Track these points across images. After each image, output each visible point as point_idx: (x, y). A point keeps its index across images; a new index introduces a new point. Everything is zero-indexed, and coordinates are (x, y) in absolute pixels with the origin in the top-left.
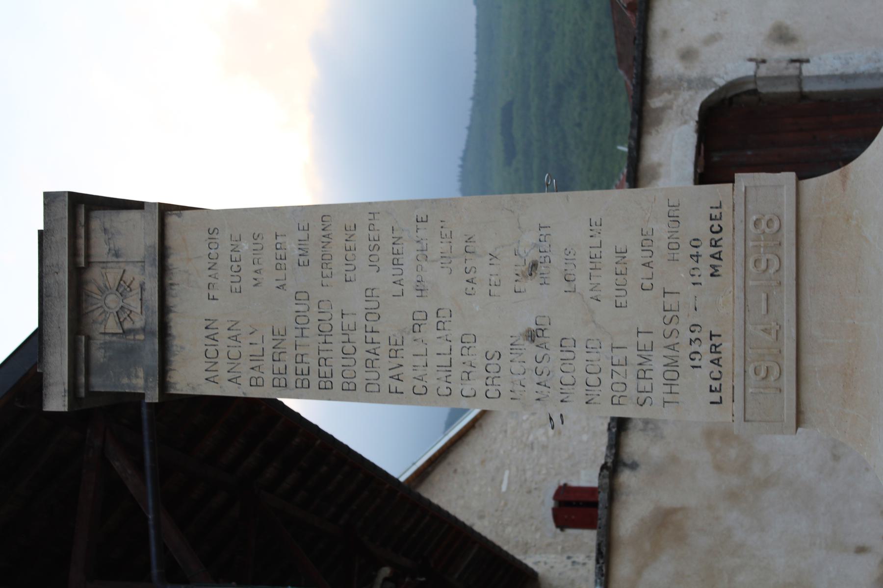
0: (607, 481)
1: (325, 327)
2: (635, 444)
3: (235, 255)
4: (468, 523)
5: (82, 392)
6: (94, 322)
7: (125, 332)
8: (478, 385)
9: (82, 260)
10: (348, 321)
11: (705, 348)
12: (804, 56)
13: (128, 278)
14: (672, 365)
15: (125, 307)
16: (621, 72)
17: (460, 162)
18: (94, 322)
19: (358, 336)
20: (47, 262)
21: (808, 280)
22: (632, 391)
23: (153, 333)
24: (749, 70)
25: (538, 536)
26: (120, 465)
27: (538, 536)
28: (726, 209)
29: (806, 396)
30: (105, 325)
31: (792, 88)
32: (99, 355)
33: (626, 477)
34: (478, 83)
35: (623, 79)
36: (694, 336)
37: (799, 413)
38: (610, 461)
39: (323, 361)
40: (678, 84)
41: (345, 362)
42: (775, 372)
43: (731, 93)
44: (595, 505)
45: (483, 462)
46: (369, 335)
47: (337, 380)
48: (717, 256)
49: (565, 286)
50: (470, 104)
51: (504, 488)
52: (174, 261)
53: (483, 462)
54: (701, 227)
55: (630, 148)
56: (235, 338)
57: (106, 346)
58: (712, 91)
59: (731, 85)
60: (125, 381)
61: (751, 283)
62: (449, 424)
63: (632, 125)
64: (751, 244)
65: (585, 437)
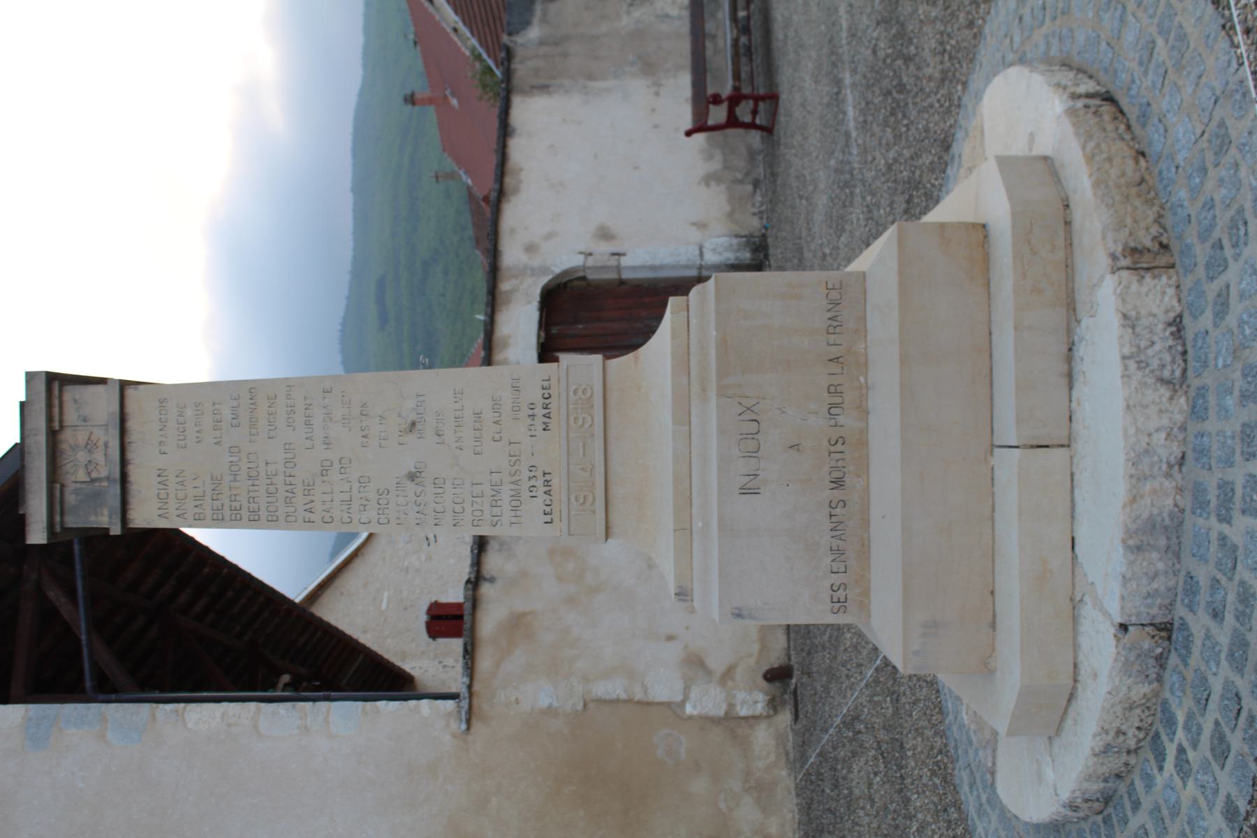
0: (470, 592)
1: (254, 473)
2: (493, 561)
3: (181, 419)
4: (355, 636)
5: (58, 528)
6: (67, 473)
7: (93, 481)
8: (372, 514)
9: (56, 425)
10: (271, 468)
11: (539, 483)
12: (620, 250)
13: (94, 438)
14: (516, 496)
15: (88, 460)
16: (478, 252)
17: (339, 327)
18: (67, 473)
19: (279, 480)
20: (28, 427)
21: (612, 433)
22: (487, 516)
23: (115, 480)
24: (578, 261)
25: (413, 645)
26: (54, 594)
27: (413, 645)
28: (554, 382)
29: (614, 516)
30: (75, 474)
31: (613, 276)
32: (71, 499)
33: (485, 589)
34: (355, 258)
35: (480, 259)
36: (531, 474)
37: (607, 528)
38: (473, 576)
39: (252, 499)
40: (522, 272)
41: (269, 500)
42: (590, 499)
43: (565, 280)
44: (461, 617)
45: (365, 585)
46: (288, 479)
47: (263, 514)
48: (547, 416)
49: (437, 439)
50: (348, 277)
51: (384, 606)
52: (131, 424)
53: (365, 585)
54: (537, 396)
55: (486, 314)
56: (182, 483)
57: (77, 492)
58: (550, 277)
59: (566, 273)
60: (93, 518)
61: (572, 435)
62: (334, 555)
63: (487, 305)
64: (571, 407)
65: (452, 561)
